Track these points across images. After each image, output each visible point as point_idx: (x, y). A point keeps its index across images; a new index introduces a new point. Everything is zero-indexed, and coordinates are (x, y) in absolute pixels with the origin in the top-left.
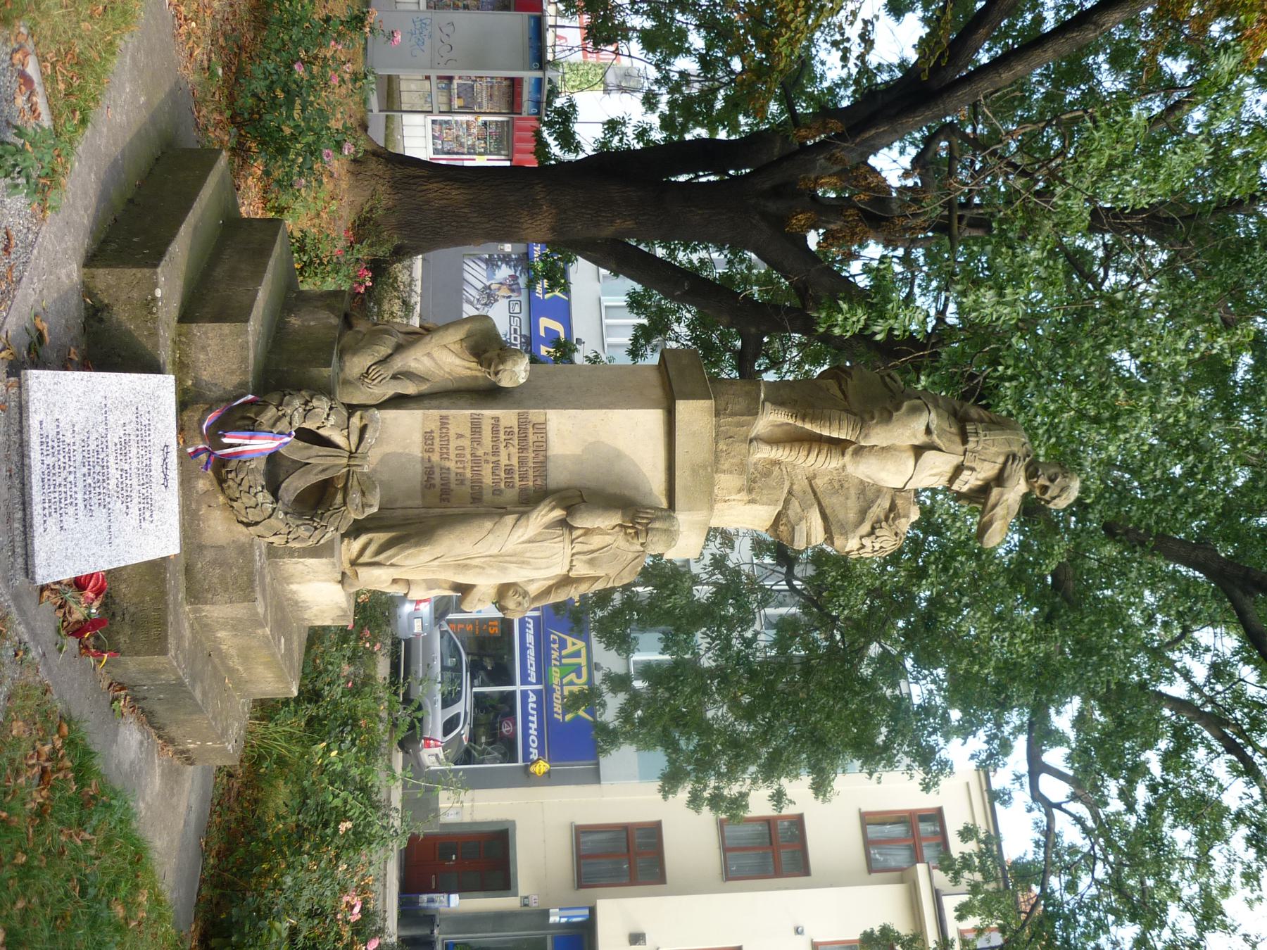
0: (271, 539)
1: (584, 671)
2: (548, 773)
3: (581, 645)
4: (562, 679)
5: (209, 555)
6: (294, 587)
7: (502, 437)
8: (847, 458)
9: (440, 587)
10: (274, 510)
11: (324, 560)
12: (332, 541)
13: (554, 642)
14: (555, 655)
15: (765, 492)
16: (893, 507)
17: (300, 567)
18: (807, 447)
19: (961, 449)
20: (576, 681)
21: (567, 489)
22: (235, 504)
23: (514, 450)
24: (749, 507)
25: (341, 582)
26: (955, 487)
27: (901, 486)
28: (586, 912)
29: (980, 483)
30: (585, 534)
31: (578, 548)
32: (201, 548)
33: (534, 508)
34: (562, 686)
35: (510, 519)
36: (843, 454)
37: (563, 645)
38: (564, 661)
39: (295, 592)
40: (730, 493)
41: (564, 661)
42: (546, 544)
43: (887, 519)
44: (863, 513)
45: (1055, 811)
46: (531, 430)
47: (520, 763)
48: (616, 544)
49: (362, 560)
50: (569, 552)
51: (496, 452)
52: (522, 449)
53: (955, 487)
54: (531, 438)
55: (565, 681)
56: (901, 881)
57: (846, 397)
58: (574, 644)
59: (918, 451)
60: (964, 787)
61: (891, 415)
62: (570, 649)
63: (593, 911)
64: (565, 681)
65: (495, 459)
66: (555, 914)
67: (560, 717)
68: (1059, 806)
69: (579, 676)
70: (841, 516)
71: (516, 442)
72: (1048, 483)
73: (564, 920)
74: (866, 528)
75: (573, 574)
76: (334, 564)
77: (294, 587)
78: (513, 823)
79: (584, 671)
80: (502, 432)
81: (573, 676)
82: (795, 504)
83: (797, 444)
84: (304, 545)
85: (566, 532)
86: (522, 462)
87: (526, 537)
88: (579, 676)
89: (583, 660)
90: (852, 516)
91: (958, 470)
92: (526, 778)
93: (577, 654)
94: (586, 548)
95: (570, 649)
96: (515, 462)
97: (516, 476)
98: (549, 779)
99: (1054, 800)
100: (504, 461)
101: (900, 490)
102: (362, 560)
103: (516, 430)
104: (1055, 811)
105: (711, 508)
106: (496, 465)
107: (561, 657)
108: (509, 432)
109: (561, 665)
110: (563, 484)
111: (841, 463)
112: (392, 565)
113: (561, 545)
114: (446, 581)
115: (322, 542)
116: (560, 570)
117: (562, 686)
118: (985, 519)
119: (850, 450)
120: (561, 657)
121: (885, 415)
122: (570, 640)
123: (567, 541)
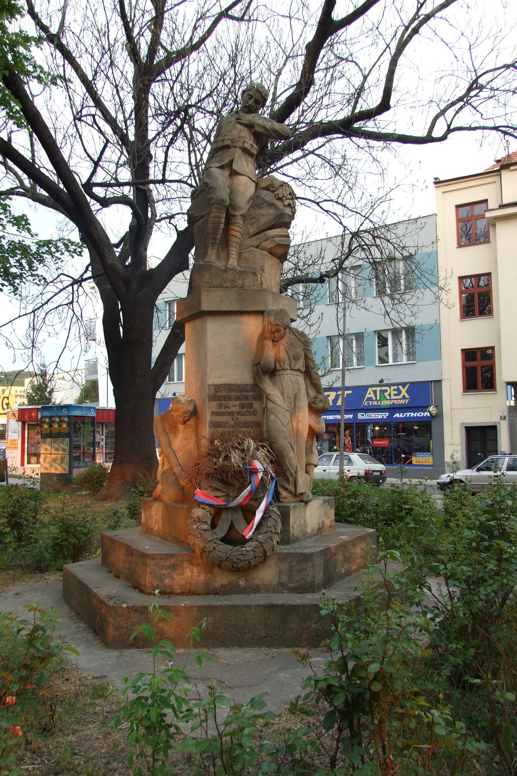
0: (275, 542)
1: (383, 388)
2: (436, 407)
3: (370, 390)
4: (387, 400)
5: (284, 579)
6: (309, 530)
7: (223, 410)
8: (237, 214)
9: (312, 447)
10: (256, 540)
11: (291, 512)
12: (279, 508)
13: (368, 403)
14: (375, 403)
15: (256, 261)
16: (267, 188)
17: (295, 526)
18: (230, 237)
19: (232, 149)
20: (388, 392)
21: (253, 372)
22: (253, 563)
23: (231, 403)
24: (266, 270)
25: (306, 503)
26: (255, 152)
27: (253, 184)
28: (509, 387)
29: (252, 139)
30: (279, 362)
31: (287, 366)
32: (281, 584)
33: (265, 392)
34: (391, 400)
35: (270, 405)
36: (235, 216)
37: (370, 399)
38: (378, 398)
39: (313, 530)
40: (257, 280)
41: (378, 398)
42: (284, 385)
43: (273, 192)
44: (271, 205)
45: (451, 128)
46: (219, 394)
47: (377, 364)
48: (285, 345)
49: (293, 491)
50: (289, 372)
51: (232, 414)
52: (229, 398)
53: (255, 152)
54: (224, 393)
55: (388, 398)
56: (494, 226)
57: (203, 216)
58: (370, 394)
59: (234, 173)
60: (445, 194)
61: (211, 188)
62: (372, 395)
63: (508, 384)
64: (388, 398)
65: (236, 415)
66: (510, 403)
67: (407, 400)
68: (449, 126)
69: (386, 391)
70: (272, 217)
71: (226, 402)
72: (253, 99)
73: (513, 398)
74: (279, 204)
75: (303, 370)
76: (295, 507)
77: (309, 530)
78: (462, 424)
79: (383, 388)
80: (220, 410)
81: (386, 394)
82: (265, 244)
83: (229, 244)
84: (280, 524)
85: (277, 373)
86: (237, 399)
87: (280, 396)
88: (386, 391)
89: (378, 389)
90: (272, 211)
91: (246, 151)
92: (439, 416)
93: (375, 392)
94: (287, 362)
95: (372, 395)
96: (237, 403)
97: (246, 402)
98: (439, 406)
99: (446, 128)
100: (237, 409)
101: (257, 184)
102: (293, 491)
103: (219, 402)
104: (451, 128)
105: (265, 290)
106: (239, 413)
107: (376, 400)
108: (221, 406)
109: (380, 400)
110: (251, 375)
111: (239, 217)
112: (296, 473)
113: (285, 376)
114: (307, 442)
115: (278, 513)
116: (301, 379)
117: (391, 400)
118: (273, 134)
119: (232, 212)
120: (376, 400)
121: (211, 191)
122: (367, 396)
123: (283, 372)
